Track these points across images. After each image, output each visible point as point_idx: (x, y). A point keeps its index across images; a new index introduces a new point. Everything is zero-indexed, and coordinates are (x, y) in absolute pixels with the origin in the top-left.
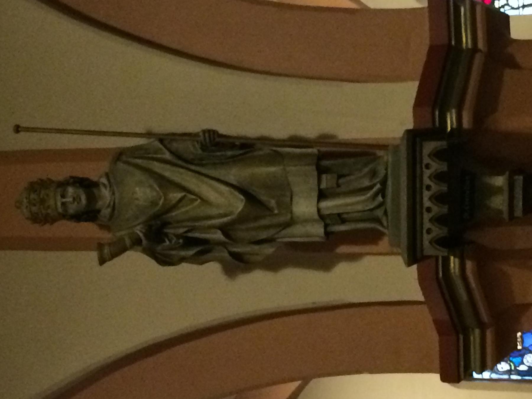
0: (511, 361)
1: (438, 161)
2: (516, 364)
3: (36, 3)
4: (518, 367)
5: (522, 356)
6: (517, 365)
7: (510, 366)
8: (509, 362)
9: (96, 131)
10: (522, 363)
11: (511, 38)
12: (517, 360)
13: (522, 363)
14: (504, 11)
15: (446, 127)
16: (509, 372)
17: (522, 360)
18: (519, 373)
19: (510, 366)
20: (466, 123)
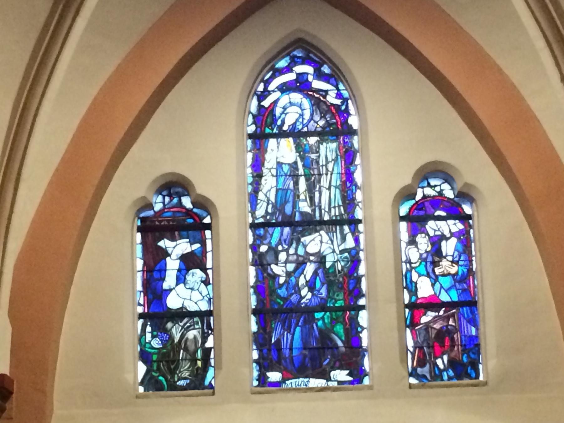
0: (421, 263)
1: (163, 300)
2: (418, 268)
3: (276, 379)
4: (416, 271)
5: (428, 275)
6: (417, 270)
7: (415, 263)
8: (420, 261)
9: (12, 214)
10: (420, 275)
11: (147, 367)
12: (422, 270)
13: (420, 275)
14: (188, 233)
15: (271, 341)
16: (409, 262)
17: (423, 275)
18: (409, 271)
19: (415, 263)
20: (146, 311)
